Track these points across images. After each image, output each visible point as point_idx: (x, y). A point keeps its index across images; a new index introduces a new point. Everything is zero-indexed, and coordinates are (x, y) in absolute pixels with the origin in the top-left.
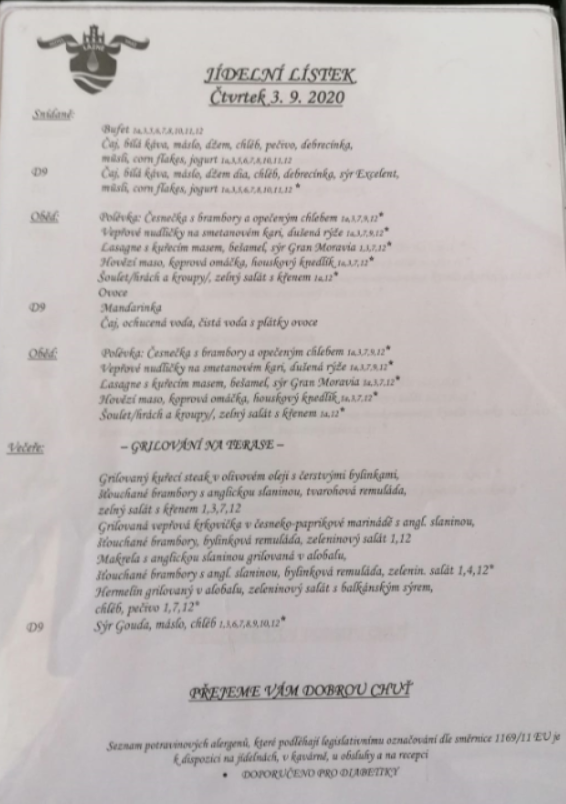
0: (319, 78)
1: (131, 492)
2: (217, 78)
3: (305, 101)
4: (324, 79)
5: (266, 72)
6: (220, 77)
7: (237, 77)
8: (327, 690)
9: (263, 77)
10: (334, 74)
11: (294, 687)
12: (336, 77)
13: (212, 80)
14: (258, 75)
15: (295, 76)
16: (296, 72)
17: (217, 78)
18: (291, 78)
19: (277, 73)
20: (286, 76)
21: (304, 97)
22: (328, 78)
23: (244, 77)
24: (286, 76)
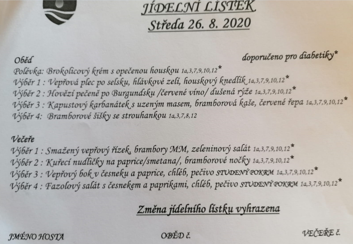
0: (227, 8)
1: (145, 113)
2: (151, 11)
3: (220, 27)
4: (231, 9)
5: (187, 5)
6: (153, 10)
7: (166, 10)
8: (168, 236)
9: (185, 9)
10: (239, 5)
11: (271, 171)
12: (240, 7)
13: (147, 13)
14: (181, 7)
15: (209, 8)
16: (180, 5)
17: (151, 11)
18: (206, 10)
19: (196, 5)
20: (202, 8)
21: (220, 22)
22: (234, 8)
23: (171, 9)
24: (202, 8)
